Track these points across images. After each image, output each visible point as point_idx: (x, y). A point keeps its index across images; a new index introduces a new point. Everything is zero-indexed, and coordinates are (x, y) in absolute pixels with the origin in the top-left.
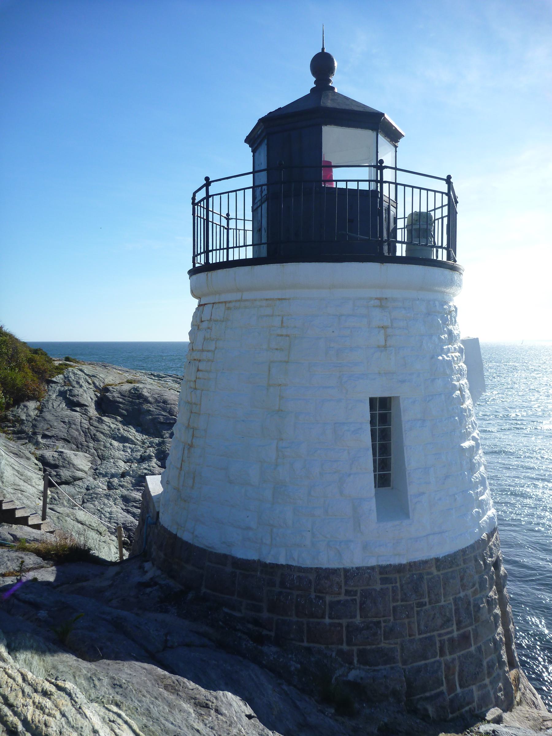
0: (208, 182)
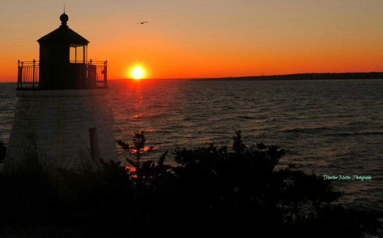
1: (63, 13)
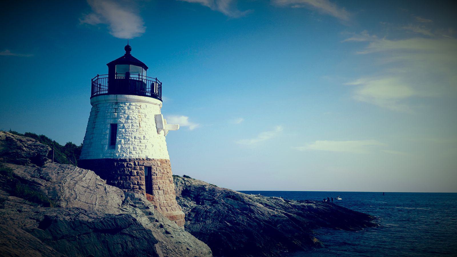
0: (98, 76)
1: (127, 45)
